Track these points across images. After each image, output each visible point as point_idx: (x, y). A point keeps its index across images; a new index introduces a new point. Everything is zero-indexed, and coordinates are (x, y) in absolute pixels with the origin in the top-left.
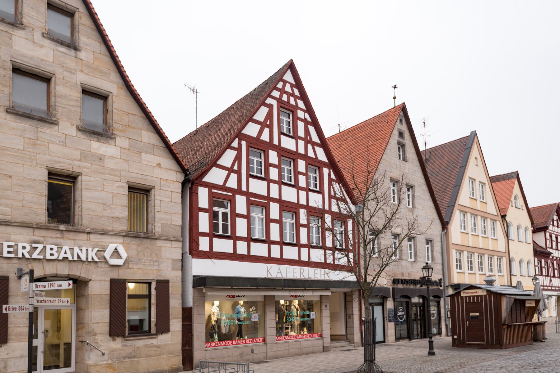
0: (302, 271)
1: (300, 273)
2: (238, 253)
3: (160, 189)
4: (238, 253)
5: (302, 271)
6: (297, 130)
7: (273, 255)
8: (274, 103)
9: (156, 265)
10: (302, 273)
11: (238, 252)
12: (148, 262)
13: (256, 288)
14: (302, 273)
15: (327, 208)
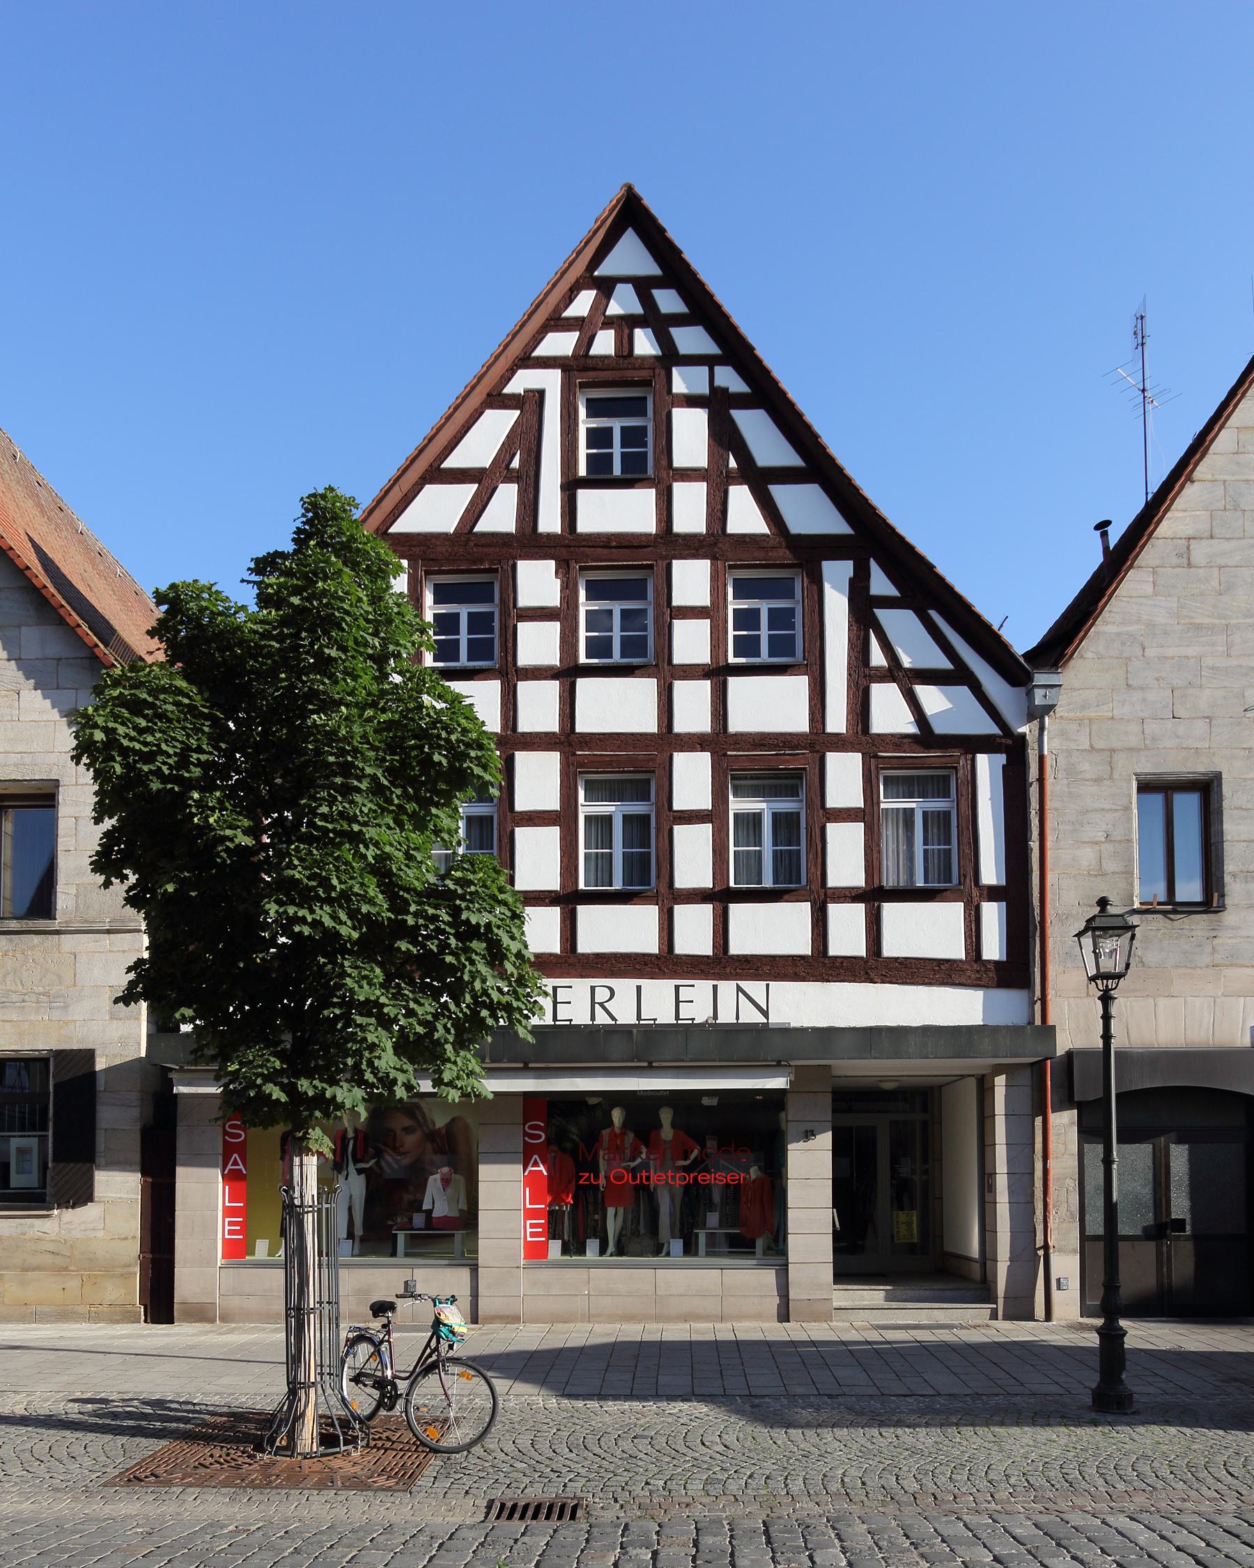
0: (602, 994)
1: (593, 1003)
2: (832, 952)
3: (77, 784)
4: (832, 952)
5: (602, 994)
6: (865, 500)
7: (837, 947)
8: (550, 382)
9: (58, 1008)
10: (601, 1004)
11: (680, 949)
12: (34, 999)
13: (521, 1065)
14: (601, 1004)
15: (837, 721)
